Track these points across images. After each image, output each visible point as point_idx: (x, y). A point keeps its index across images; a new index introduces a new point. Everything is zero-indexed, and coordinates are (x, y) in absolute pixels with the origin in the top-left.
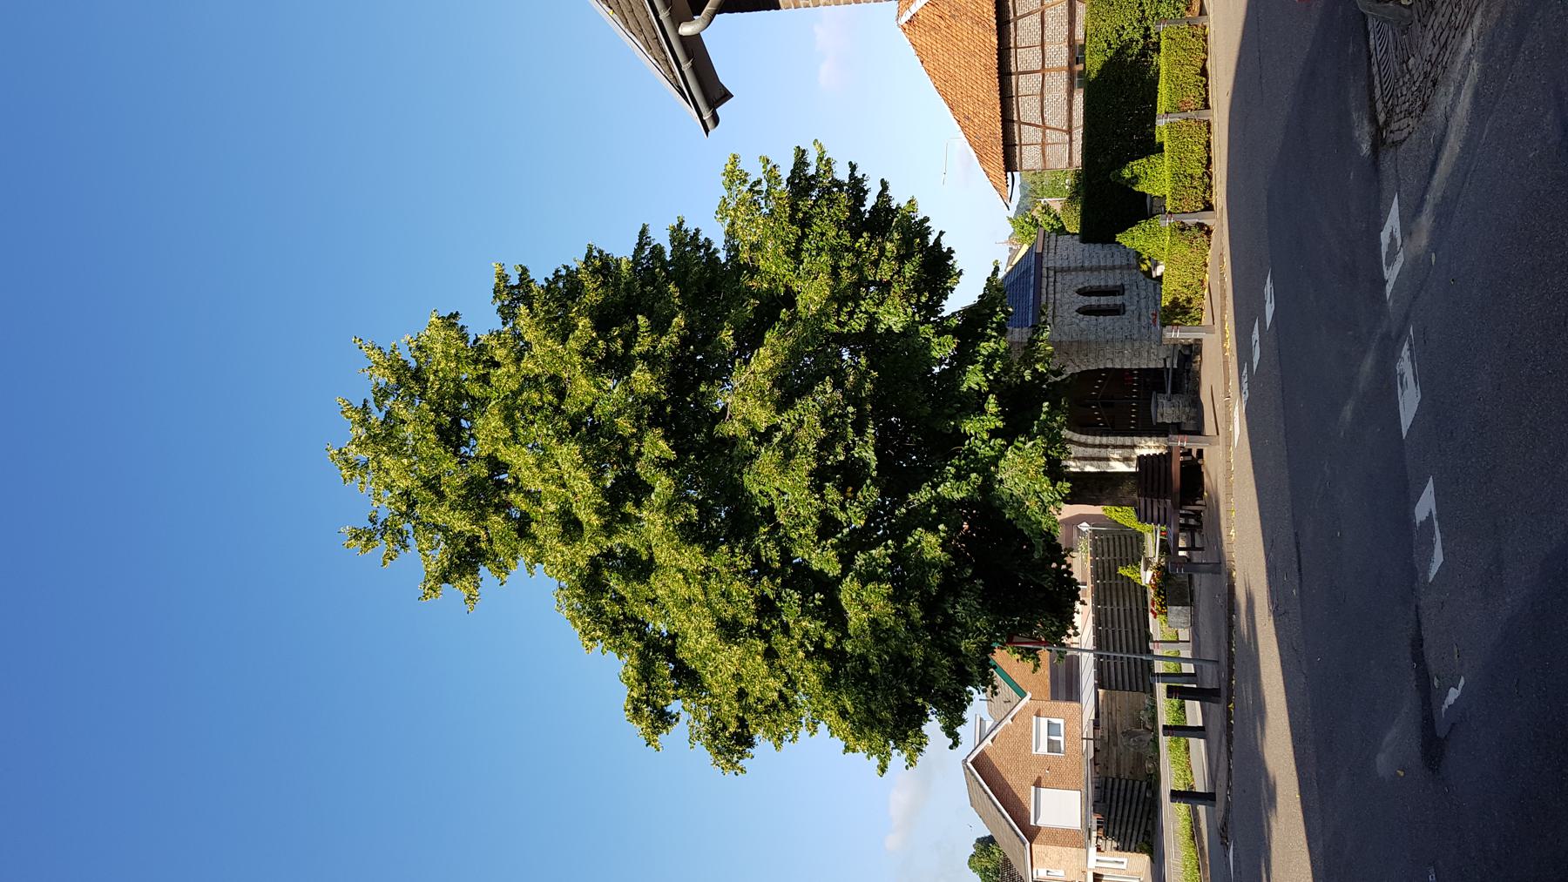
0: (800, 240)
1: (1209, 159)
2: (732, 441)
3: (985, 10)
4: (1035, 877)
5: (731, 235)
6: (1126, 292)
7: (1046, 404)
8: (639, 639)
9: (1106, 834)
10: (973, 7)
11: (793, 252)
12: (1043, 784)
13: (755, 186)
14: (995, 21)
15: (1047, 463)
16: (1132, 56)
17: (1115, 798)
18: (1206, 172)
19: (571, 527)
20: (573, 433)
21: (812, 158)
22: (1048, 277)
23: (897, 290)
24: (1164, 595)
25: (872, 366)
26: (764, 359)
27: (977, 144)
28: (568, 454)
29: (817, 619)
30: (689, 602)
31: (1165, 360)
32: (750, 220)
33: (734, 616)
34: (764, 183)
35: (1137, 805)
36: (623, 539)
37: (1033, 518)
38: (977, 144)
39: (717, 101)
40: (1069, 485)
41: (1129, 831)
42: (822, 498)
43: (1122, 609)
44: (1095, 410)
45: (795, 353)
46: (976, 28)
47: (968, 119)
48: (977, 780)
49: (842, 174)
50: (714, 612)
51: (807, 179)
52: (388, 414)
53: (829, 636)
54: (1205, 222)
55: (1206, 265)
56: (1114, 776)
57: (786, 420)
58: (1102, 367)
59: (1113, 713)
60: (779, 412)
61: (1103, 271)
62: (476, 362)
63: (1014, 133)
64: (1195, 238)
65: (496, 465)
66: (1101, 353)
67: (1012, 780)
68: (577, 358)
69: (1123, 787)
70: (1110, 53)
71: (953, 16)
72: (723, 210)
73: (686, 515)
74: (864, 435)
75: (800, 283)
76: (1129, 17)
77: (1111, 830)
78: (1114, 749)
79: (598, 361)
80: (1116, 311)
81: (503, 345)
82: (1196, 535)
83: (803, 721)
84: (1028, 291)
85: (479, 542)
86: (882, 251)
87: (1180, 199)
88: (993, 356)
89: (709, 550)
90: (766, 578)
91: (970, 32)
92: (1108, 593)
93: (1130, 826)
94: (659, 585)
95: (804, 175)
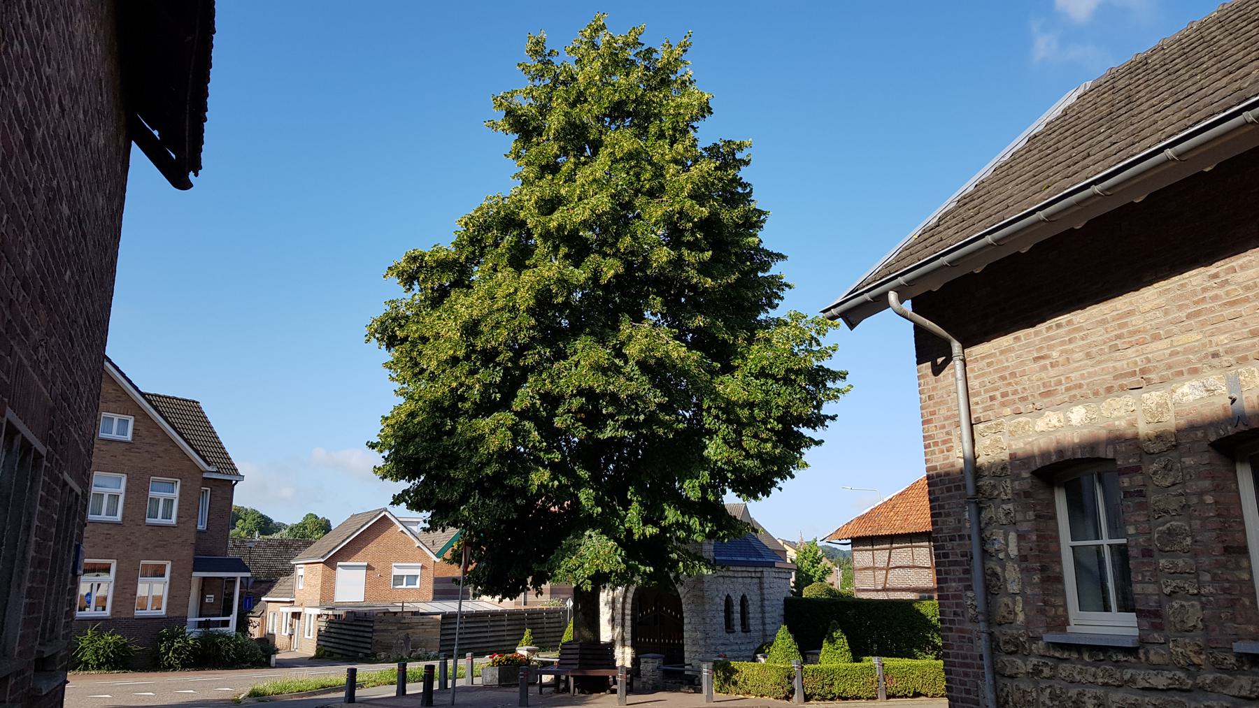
0: (773, 377)
1: (846, 699)
2: (616, 329)
4: (298, 566)
5: (779, 323)
6: (744, 634)
7: (652, 569)
8: (467, 258)
9: (330, 622)
11: (764, 372)
12: (369, 572)
13: (816, 341)
15: (605, 573)
16: (933, 637)
17: (358, 628)
19: (549, 205)
20: (620, 204)
21: (840, 384)
22: (755, 572)
23: (734, 454)
24: (507, 664)
25: (677, 432)
26: (677, 351)
28: (602, 202)
29: (481, 396)
30: (493, 298)
31: (690, 664)
32: (789, 338)
33: (482, 332)
34: (818, 348)
35: (352, 646)
36: (541, 248)
37: (563, 562)
39: (847, 319)
40: (589, 589)
41: (333, 640)
42: (573, 396)
43: (505, 633)
44: (651, 609)
45: (685, 373)
47: (893, 507)
48: (371, 520)
49: (827, 409)
50: (485, 317)
51: (822, 381)
52: (633, 63)
53: (467, 405)
54: (796, 695)
55: (762, 696)
56: (375, 628)
57: (631, 368)
58: (684, 615)
59: (423, 627)
60: (637, 363)
61: (761, 615)
62: (674, 129)
64: (783, 688)
65: (596, 146)
66: (695, 614)
67: (372, 547)
68: (677, 207)
69: (366, 635)
72: (797, 317)
73: (557, 294)
74: (623, 428)
75: (740, 377)
77: (333, 625)
78: (395, 628)
79: (676, 223)
80: (729, 626)
81: (686, 150)
82: (553, 689)
83: (406, 386)
85: (538, 135)
86: (766, 441)
88: (689, 530)
89: (531, 311)
90: (512, 355)
92: (517, 622)
93: (337, 641)
94: (505, 274)
95: (826, 379)
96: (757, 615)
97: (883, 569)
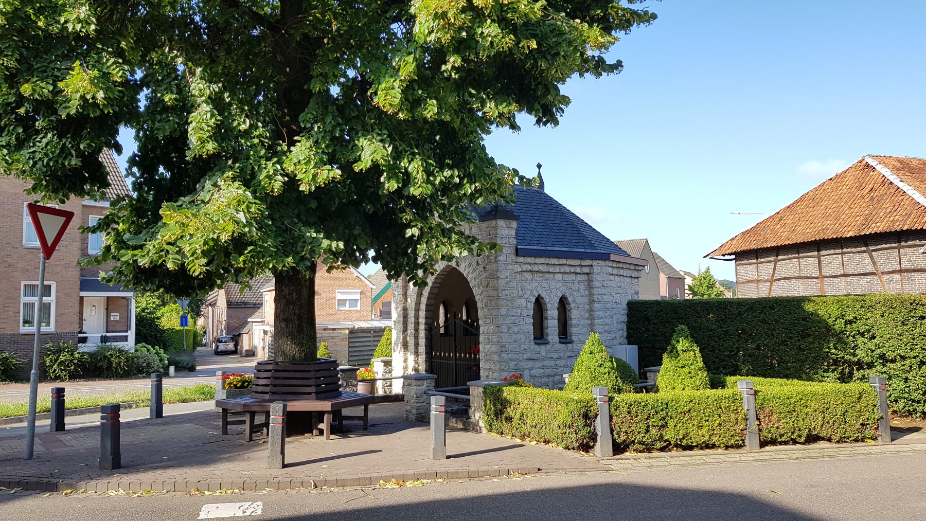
1: (690, 448)
3: (878, 224)
6: (563, 346)
10: (882, 214)
14: (868, 233)
18: (670, 444)
22: (581, 266)
27: (758, 229)
38: (758, 229)
46: (862, 218)
54: (598, 444)
58: (480, 322)
59: (333, 340)
61: (589, 322)
63: (767, 257)
70: (839, 325)
71: (872, 199)
76: (887, 345)
80: (540, 335)
84: (568, 246)
87: (629, 413)
91: (857, 214)
96: (583, 322)
97: (766, 281)
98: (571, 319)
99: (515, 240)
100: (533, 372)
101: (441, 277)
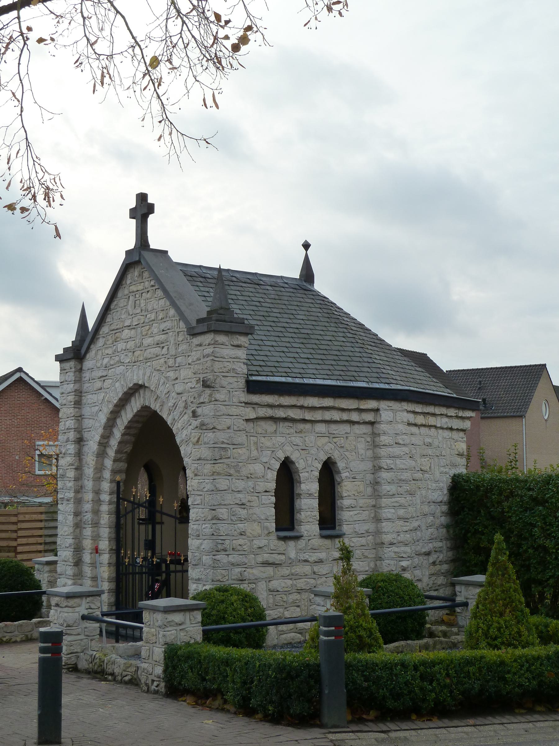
6: (328, 542)
22: (359, 410)
80: (407, 522)
84: (340, 378)
96: (361, 502)
98: (342, 498)
99: (245, 367)
100: (275, 584)
101: (135, 425)
